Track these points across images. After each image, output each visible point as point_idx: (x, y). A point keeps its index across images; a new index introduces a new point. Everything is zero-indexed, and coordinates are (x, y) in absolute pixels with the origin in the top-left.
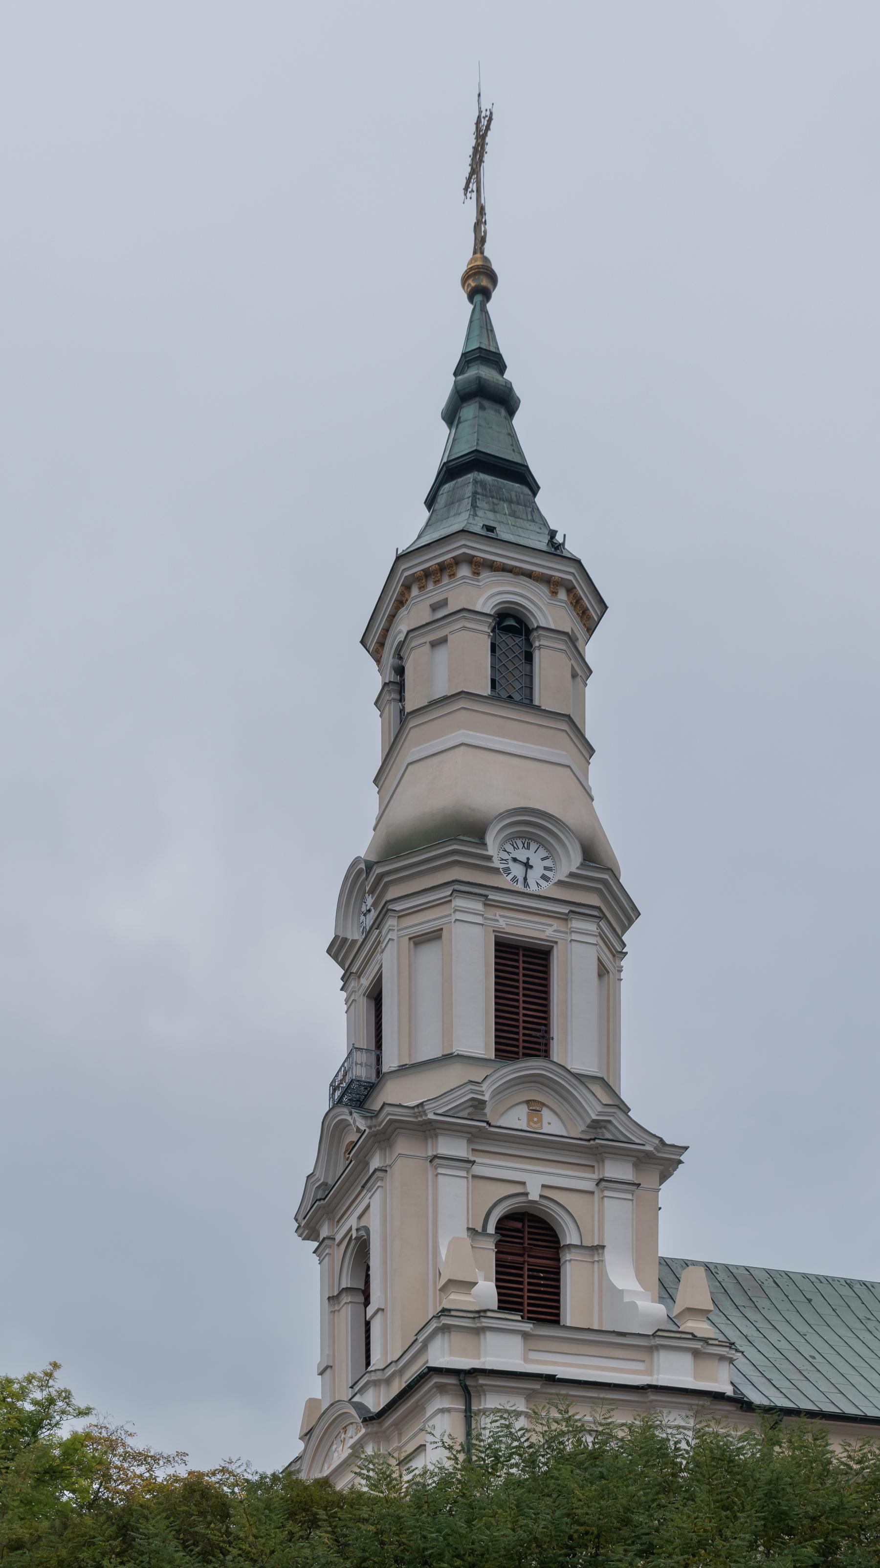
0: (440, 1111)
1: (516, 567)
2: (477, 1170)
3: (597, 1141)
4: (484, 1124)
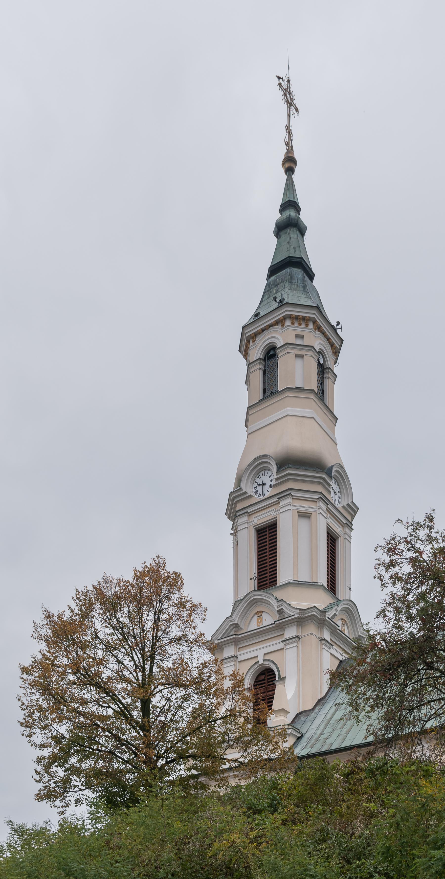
0: (219, 638)
1: (266, 326)
2: (241, 658)
3: (276, 623)
4: (234, 636)
